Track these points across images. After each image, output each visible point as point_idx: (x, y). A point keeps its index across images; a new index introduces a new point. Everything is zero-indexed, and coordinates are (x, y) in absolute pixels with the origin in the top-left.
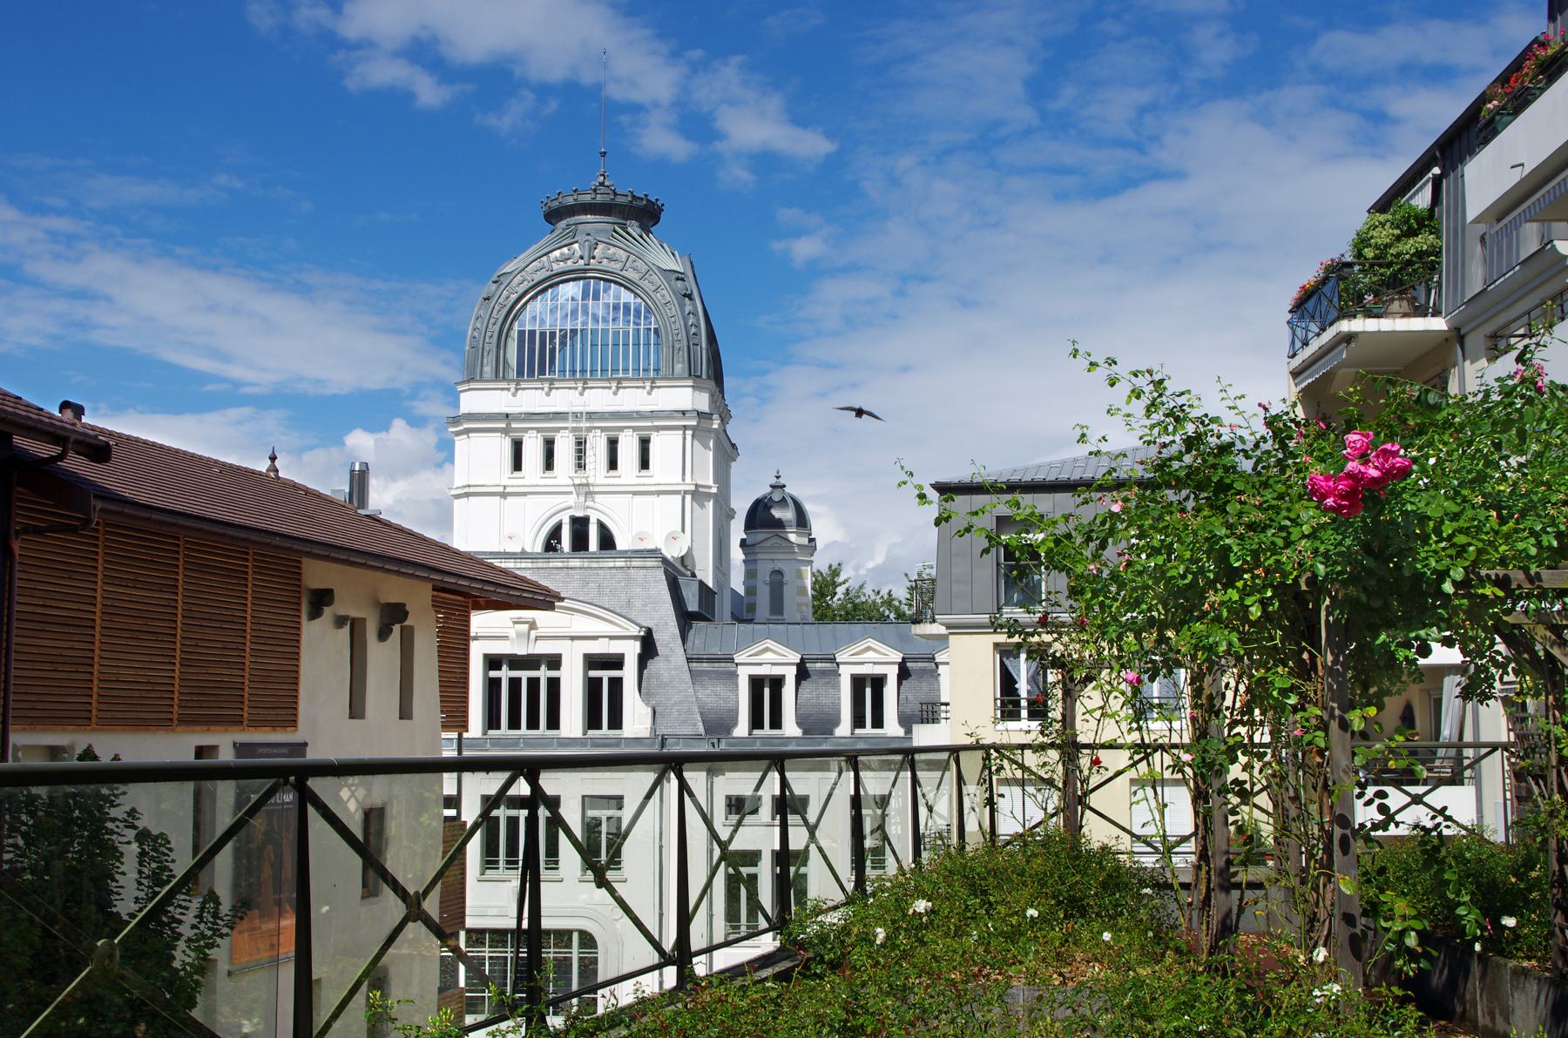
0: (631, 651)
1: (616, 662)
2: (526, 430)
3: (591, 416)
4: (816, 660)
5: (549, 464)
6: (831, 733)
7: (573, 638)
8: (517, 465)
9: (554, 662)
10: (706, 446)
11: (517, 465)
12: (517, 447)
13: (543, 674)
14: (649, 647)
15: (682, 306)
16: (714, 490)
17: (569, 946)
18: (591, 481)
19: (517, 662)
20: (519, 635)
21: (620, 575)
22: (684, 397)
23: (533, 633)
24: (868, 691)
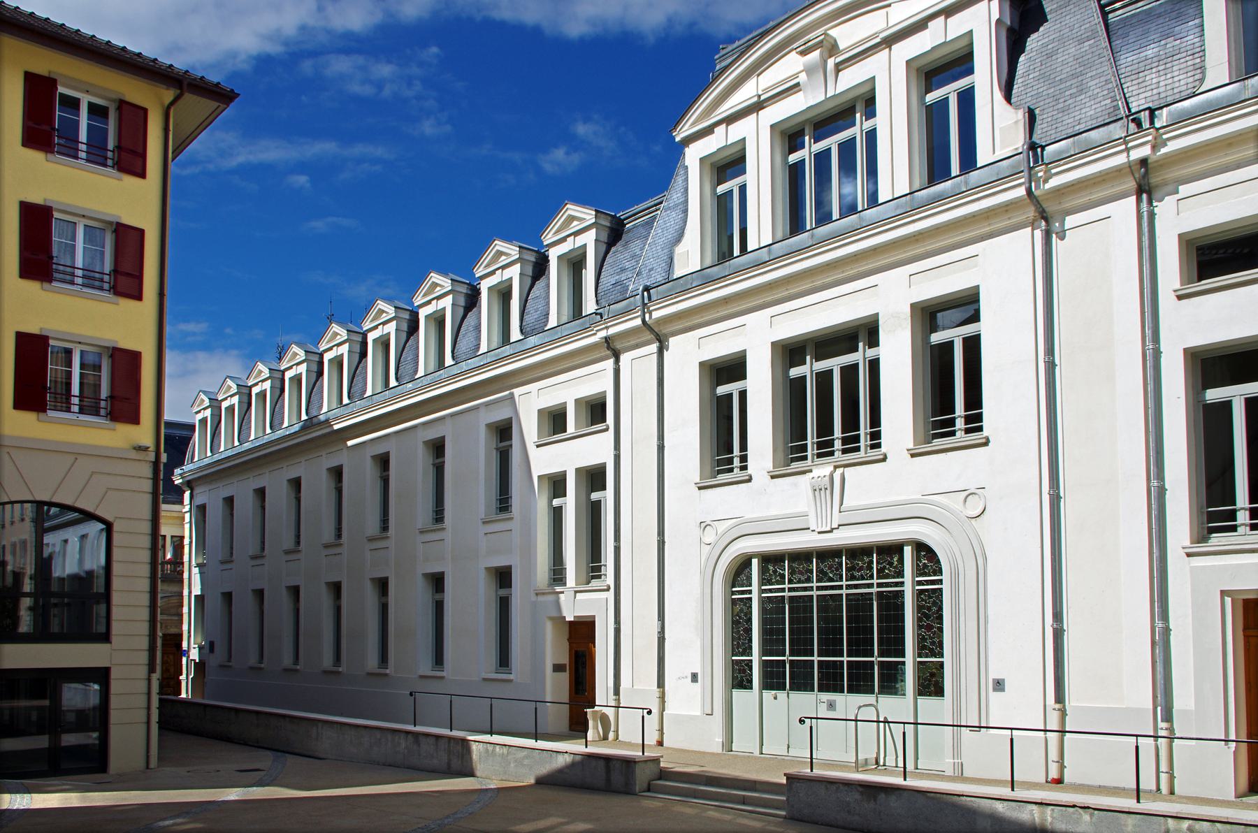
23: (831, 63)
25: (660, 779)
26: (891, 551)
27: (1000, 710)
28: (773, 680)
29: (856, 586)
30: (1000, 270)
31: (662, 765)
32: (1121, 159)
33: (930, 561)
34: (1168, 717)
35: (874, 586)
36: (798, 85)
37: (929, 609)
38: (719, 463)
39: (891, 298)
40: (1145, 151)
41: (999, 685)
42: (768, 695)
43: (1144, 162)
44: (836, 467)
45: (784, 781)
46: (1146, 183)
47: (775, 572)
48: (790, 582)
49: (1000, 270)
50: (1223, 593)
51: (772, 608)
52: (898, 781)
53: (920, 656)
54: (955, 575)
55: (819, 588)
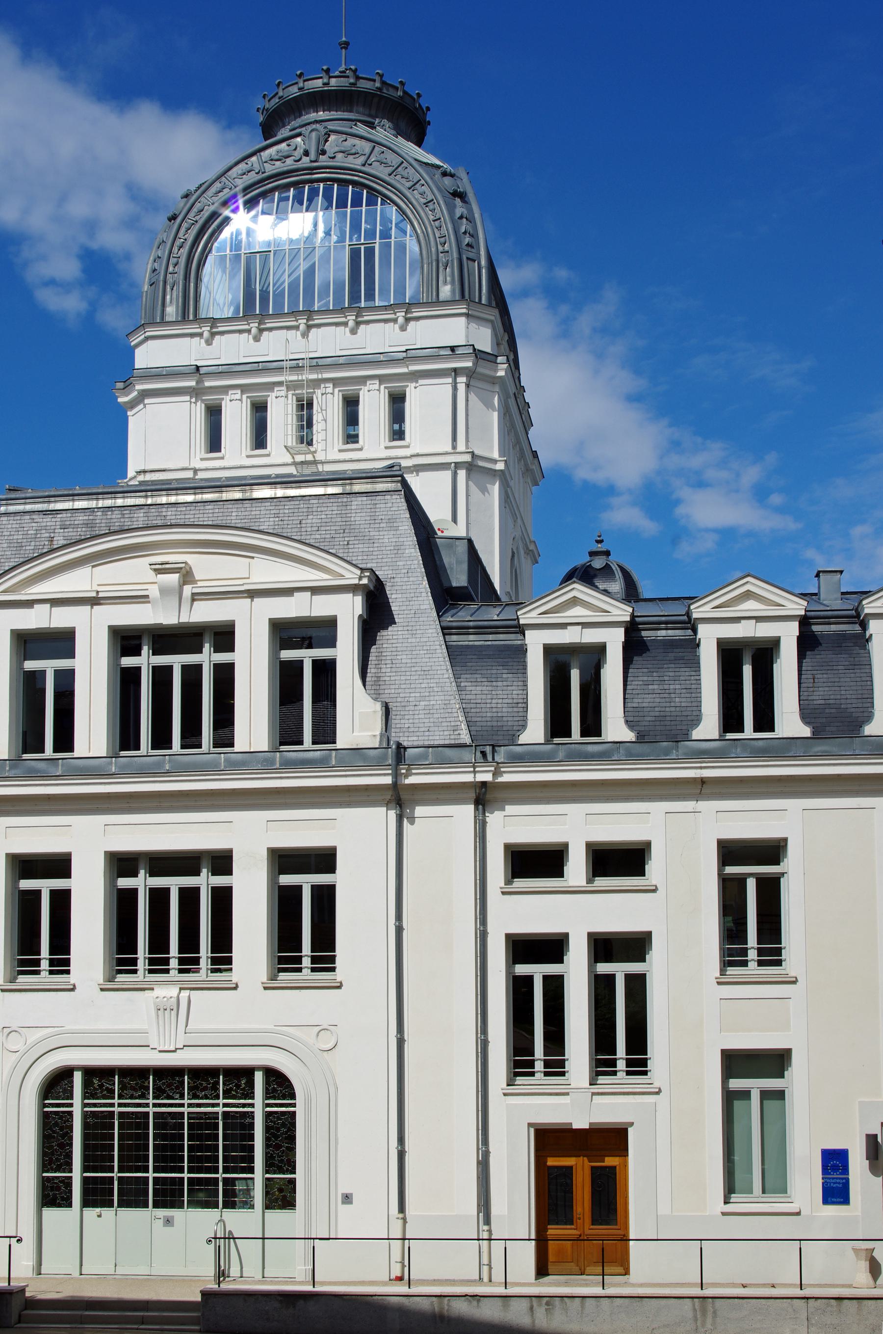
0: (348, 611)
1: (321, 631)
2: (226, 389)
3: (317, 364)
4: (656, 625)
5: (259, 439)
6: (686, 737)
7: (252, 594)
8: (214, 443)
9: (224, 636)
10: (489, 405)
11: (214, 443)
12: (214, 414)
13: (207, 658)
14: (377, 614)
15: (451, 209)
16: (500, 466)
17: (249, 1093)
18: (320, 456)
19: (167, 639)
20: (164, 591)
21: (333, 508)
22: (452, 329)
23: (188, 590)
24: (747, 671)
25: (26, 1309)
26: (239, 1078)
27: (348, 1221)
28: (97, 1195)
29: (199, 1105)
30: (358, 836)
31: (28, 1294)
32: (468, 778)
33: (280, 1085)
34: (487, 1222)
35: (220, 1106)
36: (147, 596)
37: (278, 1130)
38: (22, 963)
39: (251, 838)
40: (488, 777)
41: (347, 1199)
42: (91, 1213)
43: (484, 784)
44: (181, 989)
45: (199, 1299)
46: (483, 798)
47: (101, 1086)
48: (120, 1097)
49: (358, 836)
50: (530, 1125)
51: (97, 1126)
52: (309, 1288)
53: (267, 1172)
54: (308, 1101)
55: (155, 1105)
